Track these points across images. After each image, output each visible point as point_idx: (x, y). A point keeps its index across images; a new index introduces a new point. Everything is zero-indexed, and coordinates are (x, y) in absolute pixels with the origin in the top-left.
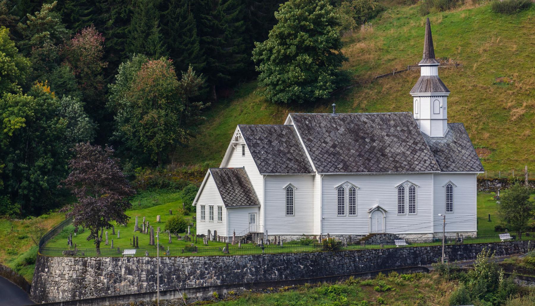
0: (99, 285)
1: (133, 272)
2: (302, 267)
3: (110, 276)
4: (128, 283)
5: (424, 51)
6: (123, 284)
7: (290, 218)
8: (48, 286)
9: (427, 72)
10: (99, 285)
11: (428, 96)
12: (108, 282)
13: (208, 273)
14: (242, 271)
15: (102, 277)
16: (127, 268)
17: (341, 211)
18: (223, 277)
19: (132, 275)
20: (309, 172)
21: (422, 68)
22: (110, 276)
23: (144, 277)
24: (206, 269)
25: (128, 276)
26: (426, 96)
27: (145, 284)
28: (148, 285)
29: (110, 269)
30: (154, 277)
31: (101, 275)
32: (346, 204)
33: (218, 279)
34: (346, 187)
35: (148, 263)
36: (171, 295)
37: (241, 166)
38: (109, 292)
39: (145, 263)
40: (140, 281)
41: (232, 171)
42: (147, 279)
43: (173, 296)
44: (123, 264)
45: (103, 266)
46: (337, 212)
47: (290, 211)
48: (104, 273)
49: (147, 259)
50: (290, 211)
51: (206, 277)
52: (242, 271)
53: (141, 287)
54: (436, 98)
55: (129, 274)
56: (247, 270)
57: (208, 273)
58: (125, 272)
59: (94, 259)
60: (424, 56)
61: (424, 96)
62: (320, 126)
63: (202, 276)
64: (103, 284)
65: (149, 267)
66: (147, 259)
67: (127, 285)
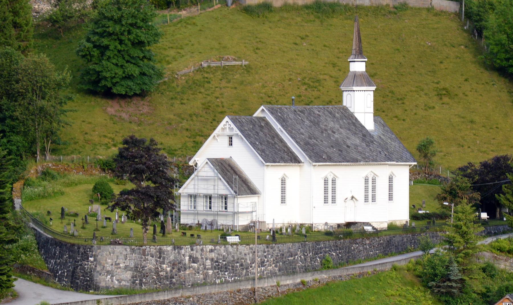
2: (334, 254)
3: (173, 265)
4: (194, 272)
5: (354, 47)
6: (187, 272)
8: (95, 274)
9: (358, 66)
12: (171, 271)
13: (268, 261)
14: (294, 259)
15: (164, 266)
16: (190, 257)
17: (326, 201)
18: (280, 264)
21: (351, 63)
22: (173, 265)
23: (209, 265)
24: (265, 257)
25: (193, 264)
27: (210, 272)
28: (214, 273)
29: (172, 257)
30: (219, 265)
31: (164, 264)
32: (330, 192)
33: (276, 266)
35: (211, 251)
36: (265, 282)
37: (229, 157)
40: (205, 269)
44: (186, 252)
48: (166, 261)
50: (391, 198)
51: (266, 265)
52: (294, 259)
53: (206, 275)
55: (194, 262)
56: (298, 258)
57: (268, 261)
58: (189, 261)
59: (154, 248)
60: (354, 52)
63: (262, 264)
65: (213, 256)
67: (192, 273)
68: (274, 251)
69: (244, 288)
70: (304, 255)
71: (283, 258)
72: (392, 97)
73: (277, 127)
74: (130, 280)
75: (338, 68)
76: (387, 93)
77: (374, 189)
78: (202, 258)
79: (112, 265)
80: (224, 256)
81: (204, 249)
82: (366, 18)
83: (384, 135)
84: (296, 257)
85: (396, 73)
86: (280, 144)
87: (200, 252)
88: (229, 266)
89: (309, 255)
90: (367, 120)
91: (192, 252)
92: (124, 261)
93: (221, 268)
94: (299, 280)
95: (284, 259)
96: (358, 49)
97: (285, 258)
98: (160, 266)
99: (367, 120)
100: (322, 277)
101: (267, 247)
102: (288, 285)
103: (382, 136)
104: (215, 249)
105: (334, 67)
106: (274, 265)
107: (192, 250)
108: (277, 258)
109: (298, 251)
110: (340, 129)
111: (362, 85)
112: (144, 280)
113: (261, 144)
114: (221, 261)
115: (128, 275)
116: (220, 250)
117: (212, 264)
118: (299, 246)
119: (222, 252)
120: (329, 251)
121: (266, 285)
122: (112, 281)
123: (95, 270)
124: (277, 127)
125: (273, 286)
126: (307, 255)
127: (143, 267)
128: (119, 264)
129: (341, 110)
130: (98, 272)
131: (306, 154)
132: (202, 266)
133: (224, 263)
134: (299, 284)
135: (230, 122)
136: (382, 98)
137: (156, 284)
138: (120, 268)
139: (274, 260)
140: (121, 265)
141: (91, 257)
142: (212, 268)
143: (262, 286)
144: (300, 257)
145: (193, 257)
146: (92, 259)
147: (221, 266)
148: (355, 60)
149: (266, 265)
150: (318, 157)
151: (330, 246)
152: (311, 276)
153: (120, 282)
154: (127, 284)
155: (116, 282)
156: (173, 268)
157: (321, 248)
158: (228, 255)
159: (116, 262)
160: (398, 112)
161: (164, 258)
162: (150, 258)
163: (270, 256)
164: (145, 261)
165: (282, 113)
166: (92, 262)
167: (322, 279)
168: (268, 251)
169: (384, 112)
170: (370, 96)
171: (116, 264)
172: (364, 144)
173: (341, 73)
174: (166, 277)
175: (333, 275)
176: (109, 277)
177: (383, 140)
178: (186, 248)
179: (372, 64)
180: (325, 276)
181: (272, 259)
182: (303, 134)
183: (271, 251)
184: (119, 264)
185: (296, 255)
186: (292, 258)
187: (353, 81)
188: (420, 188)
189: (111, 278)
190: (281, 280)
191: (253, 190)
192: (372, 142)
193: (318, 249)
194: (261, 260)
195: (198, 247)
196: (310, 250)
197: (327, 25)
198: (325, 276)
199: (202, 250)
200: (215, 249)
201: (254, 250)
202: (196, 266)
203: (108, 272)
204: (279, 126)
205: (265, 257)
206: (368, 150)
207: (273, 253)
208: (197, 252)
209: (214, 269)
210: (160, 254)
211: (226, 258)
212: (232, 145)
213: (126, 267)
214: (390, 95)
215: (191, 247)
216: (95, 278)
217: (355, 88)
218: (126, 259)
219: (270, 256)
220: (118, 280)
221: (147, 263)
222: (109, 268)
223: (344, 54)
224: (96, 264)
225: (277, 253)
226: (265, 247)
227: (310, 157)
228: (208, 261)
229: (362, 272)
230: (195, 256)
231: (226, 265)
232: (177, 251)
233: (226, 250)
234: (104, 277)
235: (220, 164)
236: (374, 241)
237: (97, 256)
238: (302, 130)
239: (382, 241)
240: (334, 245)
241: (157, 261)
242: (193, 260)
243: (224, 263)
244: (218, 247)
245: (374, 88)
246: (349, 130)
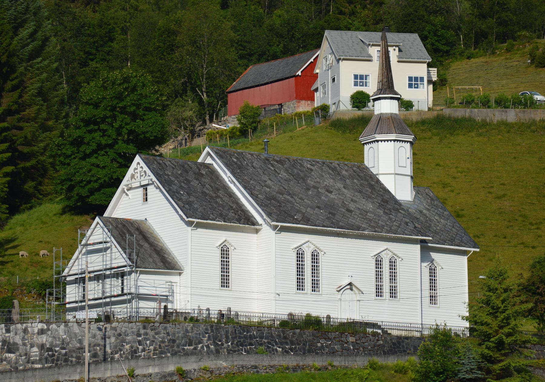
7: (225, 292)
11: (391, 140)
13: (144, 350)
17: (300, 286)
19: (14, 353)
20: (254, 224)
23: (36, 356)
24: (140, 343)
30: (53, 355)
32: (306, 272)
34: (307, 249)
35: (42, 332)
36: (106, 370)
37: (143, 218)
41: (130, 223)
46: (295, 287)
47: (225, 282)
49: (40, 326)
50: (225, 282)
52: (195, 349)
54: (401, 144)
55: (10, 351)
56: (202, 347)
57: (144, 350)
61: (385, 141)
62: (253, 166)
65: (44, 340)
66: (40, 326)
68: (156, 334)
69: (67, 378)
70: (216, 344)
71: (173, 347)
72: (524, 221)
73: (226, 175)
75: (450, 188)
76: (516, 217)
77: (393, 277)
78: (24, 344)
80: (63, 340)
81: (29, 329)
82: (506, 135)
83: (428, 210)
84: (200, 346)
85: (536, 194)
86: (226, 199)
87: (22, 334)
88: (72, 357)
89: (225, 345)
90: (402, 190)
91: (7, 335)
93: (58, 360)
94: (171, 368)
95: (175, 348)
96: (385, 80)
97: (178, 346)
99: (402, 190)
100: (219, 366)
101: (144, 328)
102: (151, 375)
103: (424, 211)
104: (48, 329)
105: (444, 187)
107: (8, 331)
108: (163, 345)
109: (204, 337)
110: (344, 190)
111: (389, 132)
113: (189, 194)
114: (57, 349)
116: (57, 331)
117: (41, 355)
118: (207, 329)
119: (61, 333)
120: (269, 343)
121: (108, 374)
124: (226, 175)
125: (122, 376)
126: (222, 344)
131: (263, 210)
132: (23, 358)
133: (64, 351)
134: (171, 374)
135: (142, 164)
136: (506, 223)
139: (155, 349)
142: (40, 360)
143: (100, 376)
144: (208, 347)
145: (9, 343)
147: (58, 357)
148: (381, 96)
149: (140, 356)
150: (285, 214)
151: (272, 336)
152: (196, 362)
157: (251, 337)
158: (71, 338)
160: (528, 238)
163: (148, 342)
165: (241, 159)
167: (218, 369)
168: (146, 334)
169: (505, 238)
172: (381, 212)
173: (452, 195)
175: (241, 363)
177: (425, 215)
179: (503, 184)
180: (224, 364)
181: (152, 348)
182: (270, 188)
183: (151, 333)
185: (200, 343)
186: (192, 347)
187: (376, 125)
190: (138, 367)
191: (170, 263)
192: (397, 210)
193: (245, 337)
194: (132, 347)
195: (19, 326)
197: (449, 143)
198: (224, 364)
199: (25, 331)
200: (48, 329)
201: (118, 331)
204: (229, 174)
205: (140, 343)
206: (385, 218)
207: (154, 337)
208: (16, 334)
209: (44, 361)
211: (68, 344)
214: (521, 219)
215: (5, 326)
217: (378, 137)
219: (148, 342)
223: (464, 174)
225: (163, 338)
226: (141, 327)
227: (269, 215)
228: (35, 349)
229: (301, 364)
230: (11, 341)
231: (66, 354)
233: (68, 332)
235: (120, 226)
236: (364, 340)
238: (269, 182)
239: (381, 342)
240: (279, 336)
243: (64, 351)
244: (54, 326)
245: (410, 138)
246: (360, 192)
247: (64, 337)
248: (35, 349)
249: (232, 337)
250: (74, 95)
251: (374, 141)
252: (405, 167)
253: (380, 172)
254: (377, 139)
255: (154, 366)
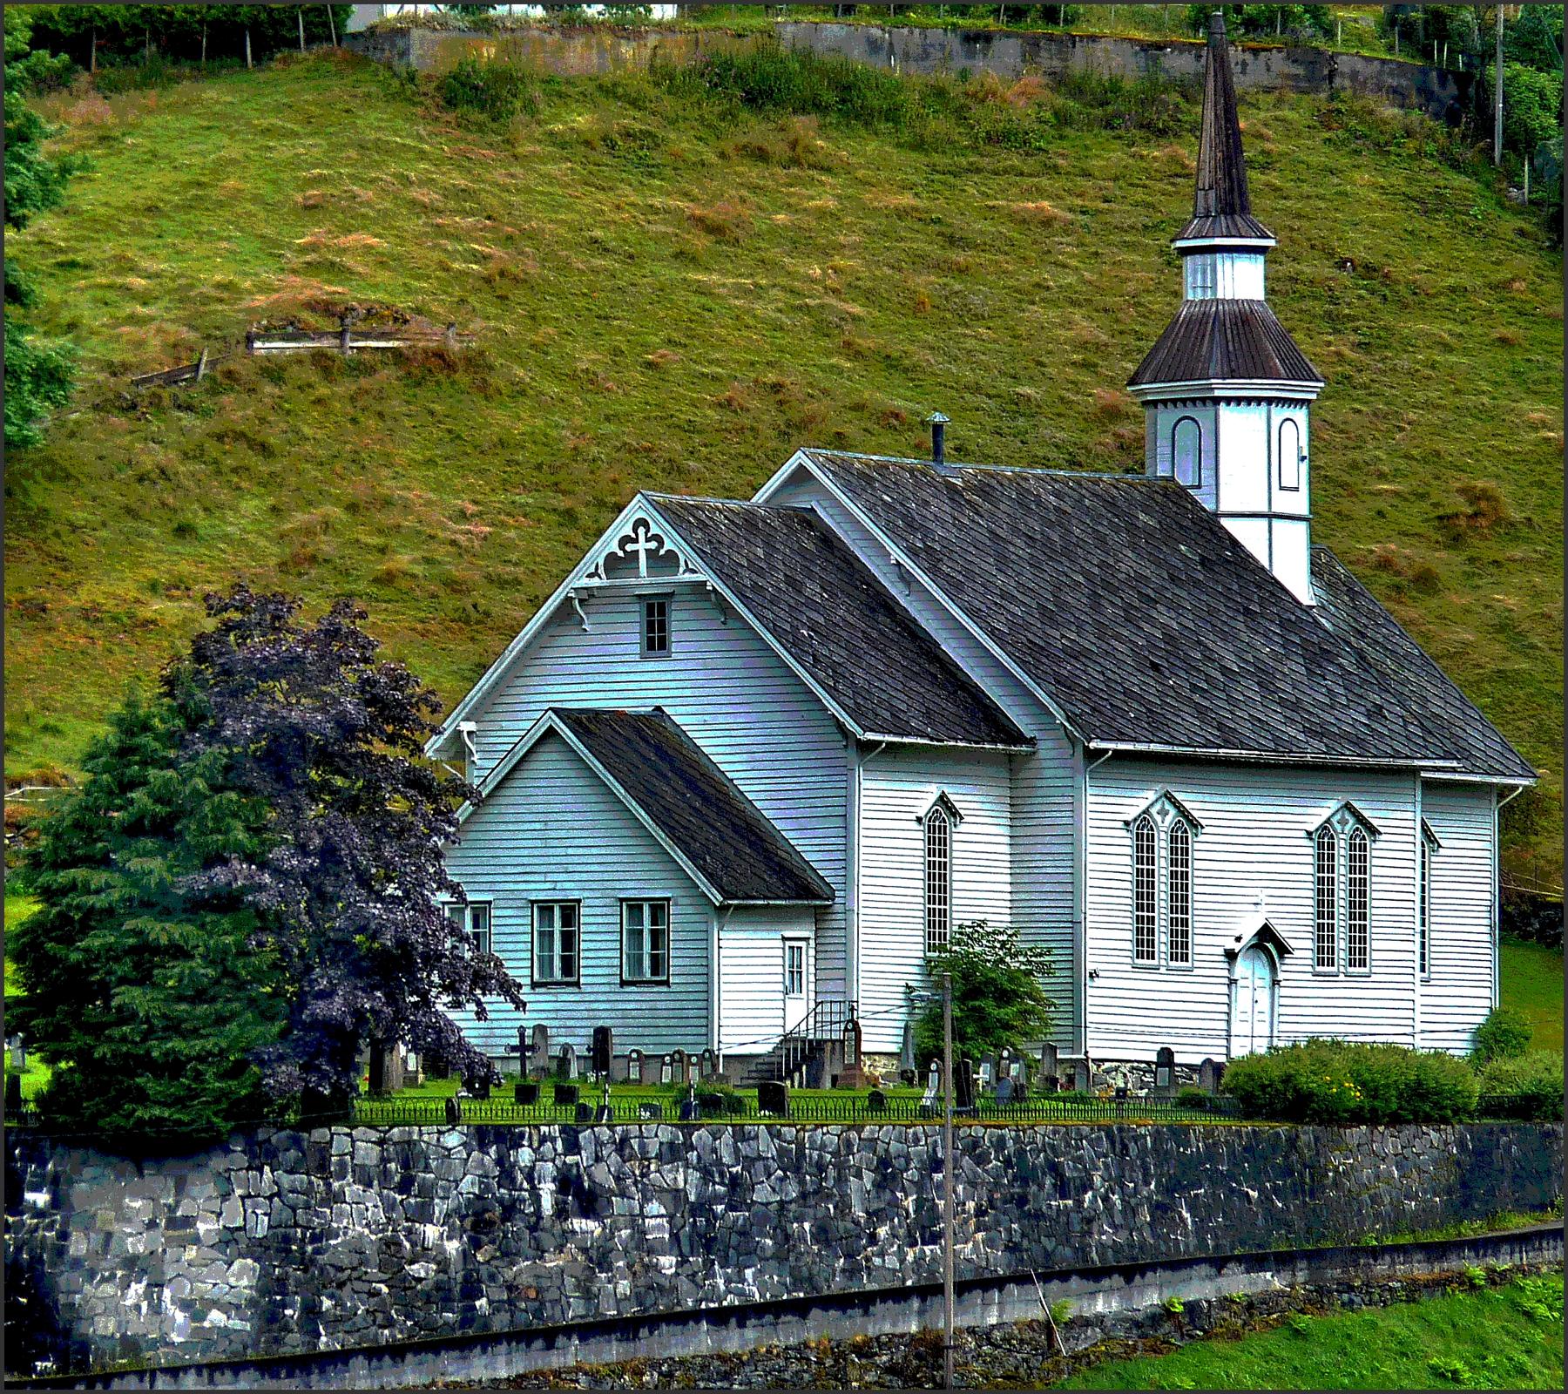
0: (418, 1269)
1: (602, 1201)
2: (1254, 1194)
3: (478, 1222)
6: (553, 1262)
10: (418, 1269)
12: (465, 1255)
15: (431, 1232)
16: (567, 1182)
23: (660, 1228)
25: (578, 1224)
26: (1249, 400)
36: (986, 1305)
38: (481, 1303)
39: (659, 1157)
42: (675, 1237)
43: (995, 1310)
45: (427, 1169)
48: (440, 1208)
64: (443, 1264)
69: (887, 1328)
74: (252, 1303)
79: (152, 1225)
81: (635, 1143)
91: (570, 1159)
92: (216, 1205)
98: (410, 1232)
102: (1100, 1320)
106: (980, 1236)
112: (327, 1303)
115: (241, 1277)
122: (156, 1309)
123: (60, 1252)
127: (316, 1238)
128: (188, 1221)
129: (1159, 498)
130: (77, 1263)
137: (390, 1323)
138: (196, 1240)
140: (202, 1227)
141: (37, 1188)
146: (41, 1199)
152: (1210, 1278)
153: (198, 1316)
154: (236, 1324)
155: (180, 1317)
156: (476, 1244)
159: (172, 1209)
161: (427, 1192)
162: (352, 1189)
164: (325, 1202)
166: (39, 1214)
170: (1295, 429)
171: (173, 1223)
174: (441, 1293)
176: (137, 1289)
178: (543, 1140)
180: (1277, 1284)
181: (971, 1205)
184: (188, 1221)
188: (1506, 951)
189: (148, 1295)
196: (1146, 1170)
202: (598, 1231)
203: (134, 1266)
210: (405, 1165)
212: (663, 644)
213: (230, 1240)
216: (62, 1299)
218: (225, 1196)
220: (185, 1305)
221: (341, 1214)
222: (136, 1245)
224: (65, 1223)
232: (493, 1150)
234: (109, 1289)
237: (71, 1183)
241: (390, 1207)
242: (581, 1196)
247: (734, 1170)
248: (655, 1207)
249: (225, 950)
250: (780, 397)
251: (1204, 400)
252: (1296, 489)
253: (1223, 508)
254: (1217, 393)
255: (1109, 1292)
